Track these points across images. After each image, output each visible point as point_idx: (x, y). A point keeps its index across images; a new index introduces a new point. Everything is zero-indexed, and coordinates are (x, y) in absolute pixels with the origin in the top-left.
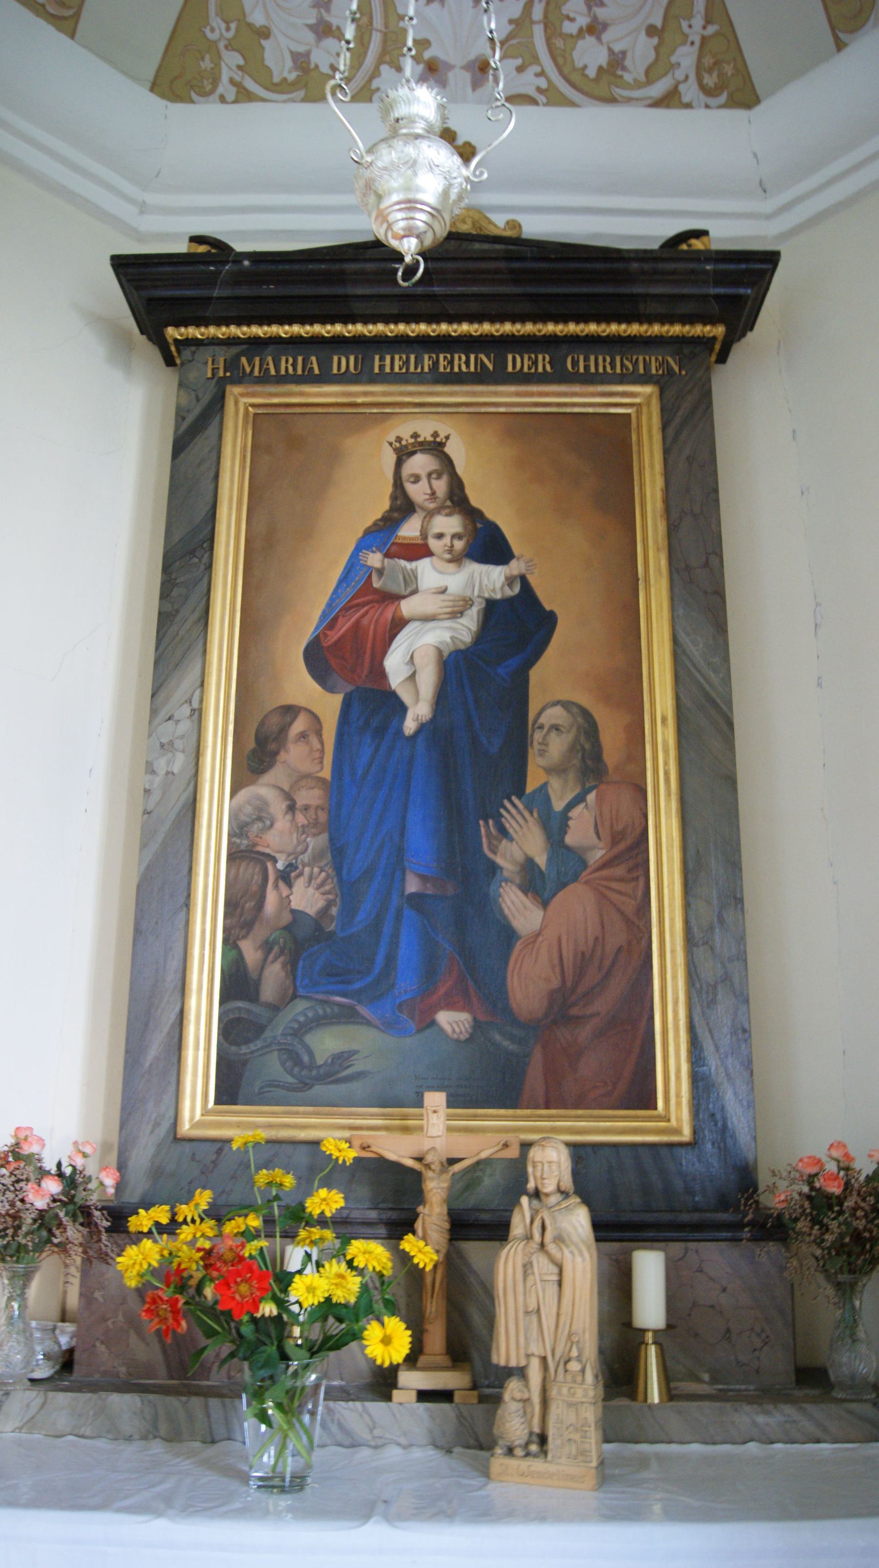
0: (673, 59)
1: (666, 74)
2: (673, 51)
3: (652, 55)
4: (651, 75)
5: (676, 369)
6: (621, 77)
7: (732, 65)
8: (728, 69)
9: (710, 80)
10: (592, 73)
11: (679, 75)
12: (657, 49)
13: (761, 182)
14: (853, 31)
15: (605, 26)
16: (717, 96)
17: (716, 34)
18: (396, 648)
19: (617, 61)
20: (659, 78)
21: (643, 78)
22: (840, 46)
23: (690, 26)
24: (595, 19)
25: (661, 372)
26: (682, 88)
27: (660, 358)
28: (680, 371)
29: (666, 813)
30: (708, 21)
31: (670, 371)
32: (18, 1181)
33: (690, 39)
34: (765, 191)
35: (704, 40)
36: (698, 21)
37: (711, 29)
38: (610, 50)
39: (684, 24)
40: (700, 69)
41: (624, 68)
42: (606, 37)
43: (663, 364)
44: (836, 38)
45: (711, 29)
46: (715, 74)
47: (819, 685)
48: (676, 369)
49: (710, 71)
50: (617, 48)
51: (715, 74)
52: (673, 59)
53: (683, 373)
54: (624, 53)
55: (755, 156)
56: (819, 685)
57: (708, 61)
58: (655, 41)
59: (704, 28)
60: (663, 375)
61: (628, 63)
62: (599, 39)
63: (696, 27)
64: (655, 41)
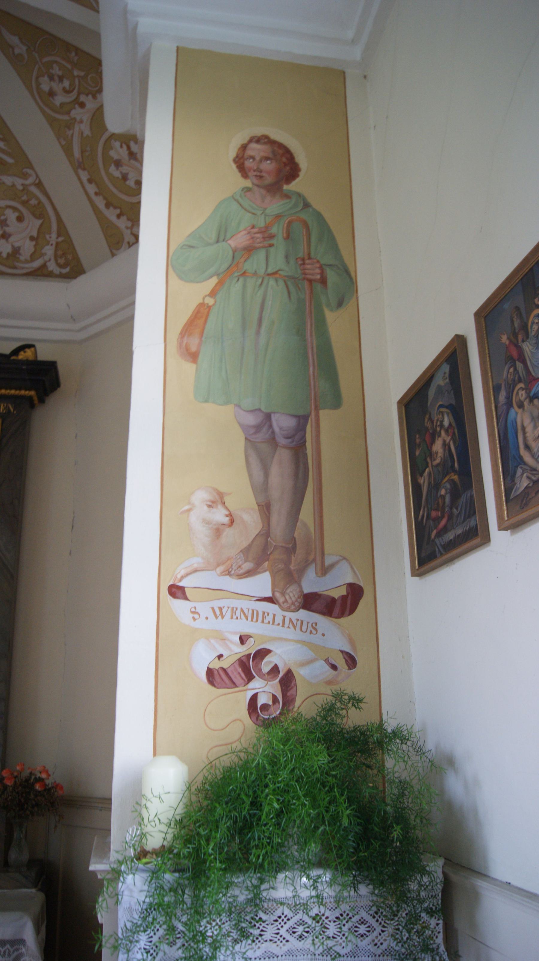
0: (43, 251)
1: (40, 257)
2: (43, 248)
3: (33, 250)
4: (33, 257)
5: (12, 410)
6: (18, 258)
7: (71, 255)
8: (70, 257)
9: (62, 261)
10: (4, 255)
11: (46, 258)
12: (35, 246)
13: (72, 317)
14: (118, 249)
15: (10, 235)
16: (66, 267)
17: (62, 242)
18: (356, 272)
19: (16, 251)
20: (38, 259)
21: (29, 258)
22: (113, 255)
23: (50, 237)
24: (5, 232)
25: (5, 411)
26: (48, 264)
27: (5, 405)
28: (14, 411)
29: (453, 456)
30: (59, 235)
31: (9, 411)
32: (219, 797)
33: (51, 243)
34: (74, 320)
35: (57, 244)
36: (54, 236)
37: (60, 239)
38: (13, 247)
39: (47, 236)
40: (56, 257)
41: (20, 254)
42: (11, 239)
43: (6, 408)
44: (111, 251)
45: (60, 239)
46: (63, 259)
47: (70, 553)
48: (12, 410)
49: (61, 257)
50: (17, 245)
51: (63, 259)
52: (43, 251)
53: (15, 412)
54: (19, 248)
55: (68, 305)
56: (70, 553)
57: (60, 253)
58: (34, 243)
59: (57, 238)
60: (6, 412)
61: (21, 251)
62: (7, 240)
63: (53, 237)
64: (34, 243)
